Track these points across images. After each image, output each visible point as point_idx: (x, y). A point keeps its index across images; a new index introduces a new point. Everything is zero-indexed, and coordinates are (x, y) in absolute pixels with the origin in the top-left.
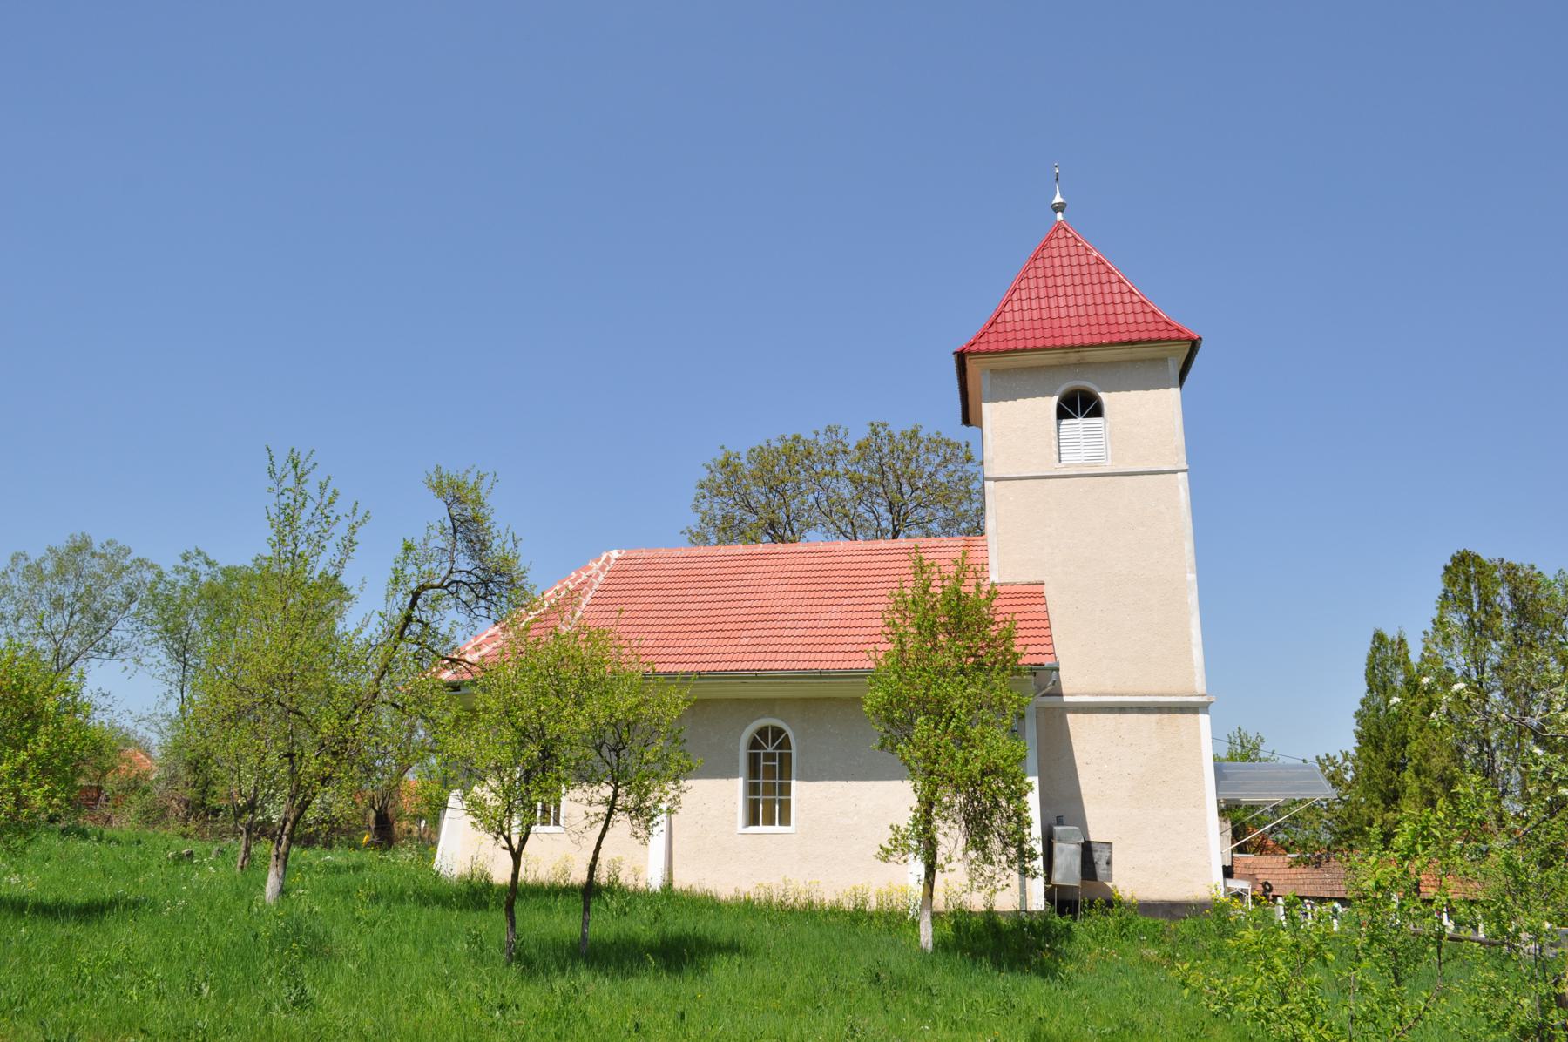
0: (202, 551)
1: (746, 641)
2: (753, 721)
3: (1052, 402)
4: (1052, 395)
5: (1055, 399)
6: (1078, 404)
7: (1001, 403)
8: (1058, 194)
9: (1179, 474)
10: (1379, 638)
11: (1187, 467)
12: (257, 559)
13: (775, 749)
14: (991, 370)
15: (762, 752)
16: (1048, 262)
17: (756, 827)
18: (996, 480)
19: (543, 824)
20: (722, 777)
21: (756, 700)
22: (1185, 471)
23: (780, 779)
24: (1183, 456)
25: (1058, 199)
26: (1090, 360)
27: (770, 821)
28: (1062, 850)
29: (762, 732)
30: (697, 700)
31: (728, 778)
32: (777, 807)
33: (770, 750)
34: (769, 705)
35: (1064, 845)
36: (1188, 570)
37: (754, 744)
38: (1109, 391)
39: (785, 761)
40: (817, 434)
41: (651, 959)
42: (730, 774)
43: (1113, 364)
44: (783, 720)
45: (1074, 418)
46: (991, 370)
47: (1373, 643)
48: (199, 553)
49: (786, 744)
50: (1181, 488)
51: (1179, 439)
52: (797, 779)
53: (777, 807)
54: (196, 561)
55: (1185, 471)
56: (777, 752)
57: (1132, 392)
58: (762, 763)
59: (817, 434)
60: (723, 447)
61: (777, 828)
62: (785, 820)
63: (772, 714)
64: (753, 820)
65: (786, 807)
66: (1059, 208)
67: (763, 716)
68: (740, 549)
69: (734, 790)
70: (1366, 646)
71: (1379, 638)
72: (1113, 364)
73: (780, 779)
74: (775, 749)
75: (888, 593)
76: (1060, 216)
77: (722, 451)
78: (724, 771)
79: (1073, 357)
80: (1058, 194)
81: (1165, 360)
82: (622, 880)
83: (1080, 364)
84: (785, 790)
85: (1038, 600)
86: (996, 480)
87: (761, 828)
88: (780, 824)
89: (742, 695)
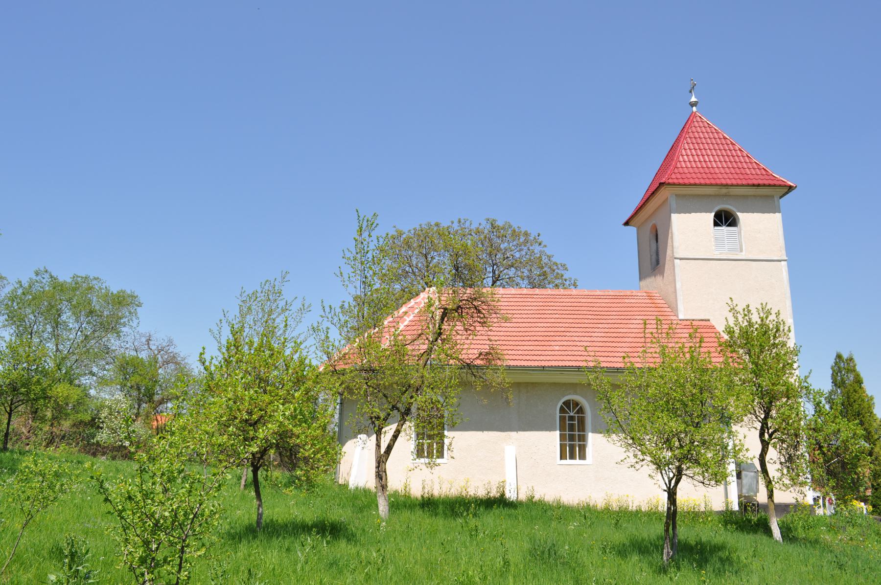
0: (49, 270)
1: (557, 348)
2: (564, 397)
3: (712, 215)
4: (711, 212)
5: (713, 214)
6: (725, 219)
7: (682, 214)
8: (693, 96)
9: (782, 262)
10: (839, 357)
11: (786, 258)
12: (74, 277)
13: (575, 414)
14: (676, 195)
15: (567, 415)
16: (691, 135)
17: (565, 460)
18: (681, 259)
19: (438, 457)
20: (546, 430)
21: (565, 384)
22: (676, 258)
23: (578, 432)
24: (784, 252)
25: (693, 99)
26: (732, 194)
27: (572, 457)
28: (746, 476)
29: (567, 403)
30: (514, 383)
31: (550, 431)
32: (577, 449)
33: (572, 414)
34: (573, 387)
35: (748, 473)
36: (789, 316)
37: (562, 410)
38: (743, 212)
39: (582, 422)
40: (452, 223)
41: (708, 547)
42: (550, 428)
43: (745, 197)
44: (582, 396)
45: (720, 226)
46: (676, 195)
47: (836, 359)
48: (46, 271)
49: (581, 411)
50: (784, 270)
51: (781, 242)
52: (448, 431)
53: (568, 448)
54: (43, 276)
55: (676, 258)
56: (576, 415)
57: (755, 214)
58: (567, 422)
59: (452, 223)
60: (395, 227)
61: (577, 461)
62: (583, 457)
63: (575, 393)
64: (563, 457)
65: (583, 449)
66: (693, 105)
67: (570, 394)
68: (513, 291)
69: (552, 439)
70: (831, 361)
71: (839, 357)
72: (745, 197)
73: (578, 432)
74: (575, 414)
75: (689, 324)
76: (694, 109)
77: (395, 229)
78: (546, 427)
79: (724, 191)
80: (693, 96)
81: (773, 197)
82: (507, 495)
83: (725, 195)
84: (442, 436)
85: (712, 330)
86: (681, 259)
87: (568, 461)
88: (580, 459)
89: (557, 381)
